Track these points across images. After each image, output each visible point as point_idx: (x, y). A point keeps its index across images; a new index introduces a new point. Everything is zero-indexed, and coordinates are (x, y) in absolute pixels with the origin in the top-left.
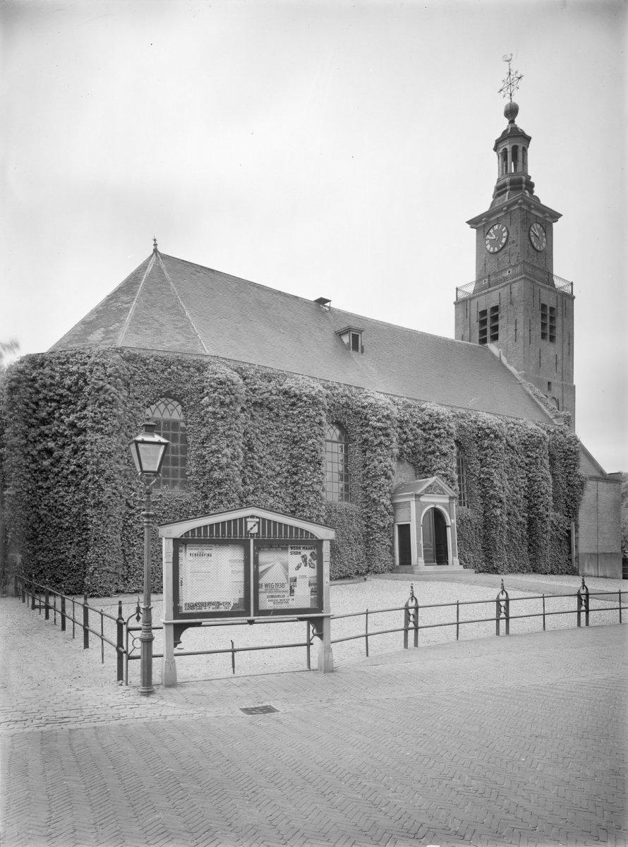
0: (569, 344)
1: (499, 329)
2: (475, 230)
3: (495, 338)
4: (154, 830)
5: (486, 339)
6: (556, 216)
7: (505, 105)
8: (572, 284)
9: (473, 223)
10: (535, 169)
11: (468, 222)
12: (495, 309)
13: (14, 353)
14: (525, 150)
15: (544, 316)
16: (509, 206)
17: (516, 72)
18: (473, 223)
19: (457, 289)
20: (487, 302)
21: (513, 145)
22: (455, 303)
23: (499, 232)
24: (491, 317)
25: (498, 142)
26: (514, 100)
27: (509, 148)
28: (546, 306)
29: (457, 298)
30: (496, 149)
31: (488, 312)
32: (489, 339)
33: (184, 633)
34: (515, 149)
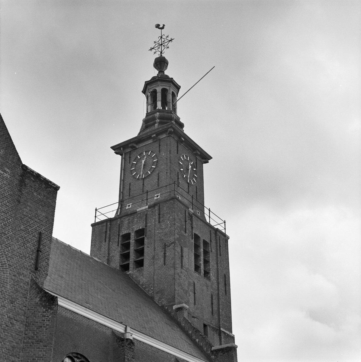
1: (145, 254)
2: (119, 157)
3: (140, 264)
5: (128, 264)
6: (206, 158)
8: (225, 222)
9: (118, 149)
10: (184, 110)
11: (113, 148)
14: (174, 96)
15: (197, 247)
17: (168, 37)
18: (118, 149)
19: (96, 210)
20: (131, 228)
21: (161, 91)
22: (93, 225)
23: (68, 245)
24: (135, 261)
25: (147, 84)
26: (163, 55)
27: (159, 89)
30: (144, 92)
31: (133, 235)
32: (131, 266)
34: (164, 91)
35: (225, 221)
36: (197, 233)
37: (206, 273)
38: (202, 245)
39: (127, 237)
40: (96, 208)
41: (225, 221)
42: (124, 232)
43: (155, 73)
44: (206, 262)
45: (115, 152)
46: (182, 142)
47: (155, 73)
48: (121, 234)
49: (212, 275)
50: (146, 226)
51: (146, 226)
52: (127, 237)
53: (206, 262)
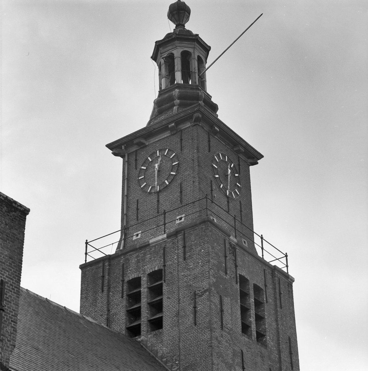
0: (291, 353)
4: (30, 337)
6: (254, 157)
7: (167, 17)
8: (286, 256)
9: (116, 147)
11: (109, 146)
12: (157, 276)
13: (116, 314)
14: (201, 62)
15: (244, 295)
16: (179, 122)
19: (87, 243)
22: (82, 267)
25: (159, 45)
27: (177, 53)
28: (247, 280)
29: (86, 261)
30: (155, 57)
31: (144, 279)
32: (144, 328)
33: (112, 254)
34: (186, 56)
35: (286, 253)
36: (243, 274)
37: (260, 336)
38: (252, 292)
39: (136, 283)
40: (87, 240)
41: (286, 253)
42: (131, 276)
43: (170, 27)
44: (259, 318)
45: (112, 153)
46: (216, 133)
47: (170, 27)
48: (126, 279)
49: (269, 338)
50: (164, 266)
51: (164, 266)
52: (136, 283)
53: (259, 318)
